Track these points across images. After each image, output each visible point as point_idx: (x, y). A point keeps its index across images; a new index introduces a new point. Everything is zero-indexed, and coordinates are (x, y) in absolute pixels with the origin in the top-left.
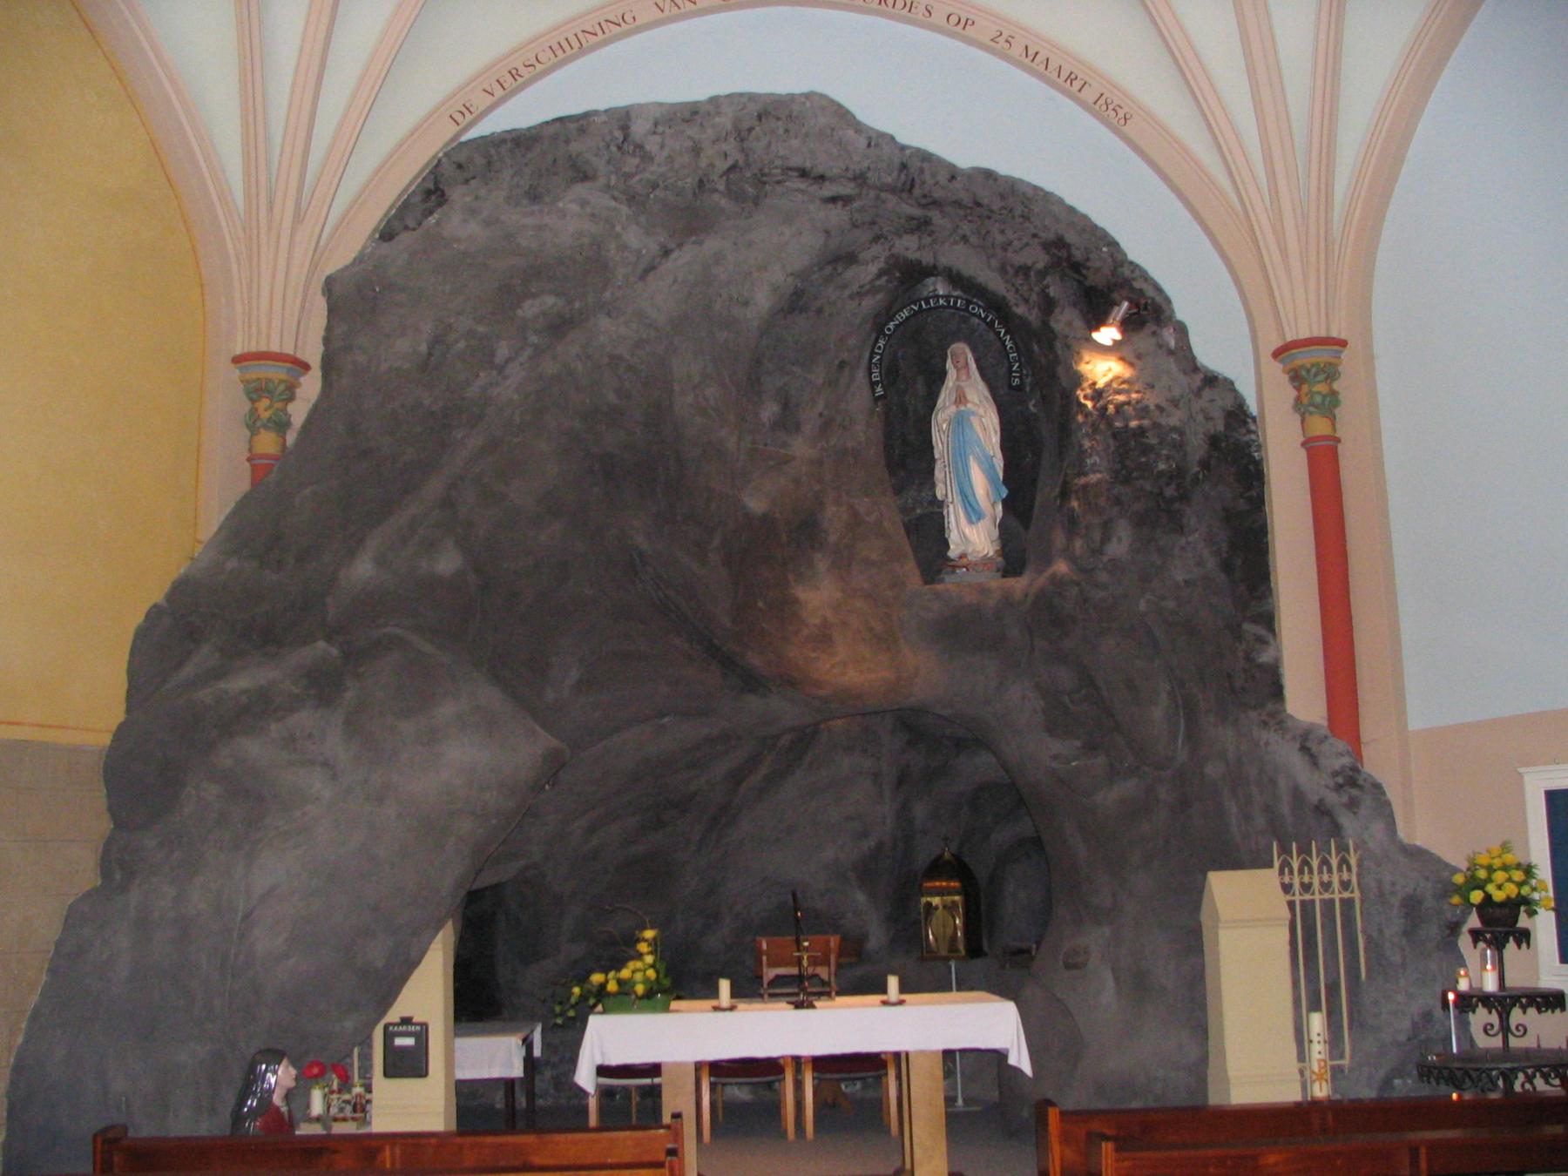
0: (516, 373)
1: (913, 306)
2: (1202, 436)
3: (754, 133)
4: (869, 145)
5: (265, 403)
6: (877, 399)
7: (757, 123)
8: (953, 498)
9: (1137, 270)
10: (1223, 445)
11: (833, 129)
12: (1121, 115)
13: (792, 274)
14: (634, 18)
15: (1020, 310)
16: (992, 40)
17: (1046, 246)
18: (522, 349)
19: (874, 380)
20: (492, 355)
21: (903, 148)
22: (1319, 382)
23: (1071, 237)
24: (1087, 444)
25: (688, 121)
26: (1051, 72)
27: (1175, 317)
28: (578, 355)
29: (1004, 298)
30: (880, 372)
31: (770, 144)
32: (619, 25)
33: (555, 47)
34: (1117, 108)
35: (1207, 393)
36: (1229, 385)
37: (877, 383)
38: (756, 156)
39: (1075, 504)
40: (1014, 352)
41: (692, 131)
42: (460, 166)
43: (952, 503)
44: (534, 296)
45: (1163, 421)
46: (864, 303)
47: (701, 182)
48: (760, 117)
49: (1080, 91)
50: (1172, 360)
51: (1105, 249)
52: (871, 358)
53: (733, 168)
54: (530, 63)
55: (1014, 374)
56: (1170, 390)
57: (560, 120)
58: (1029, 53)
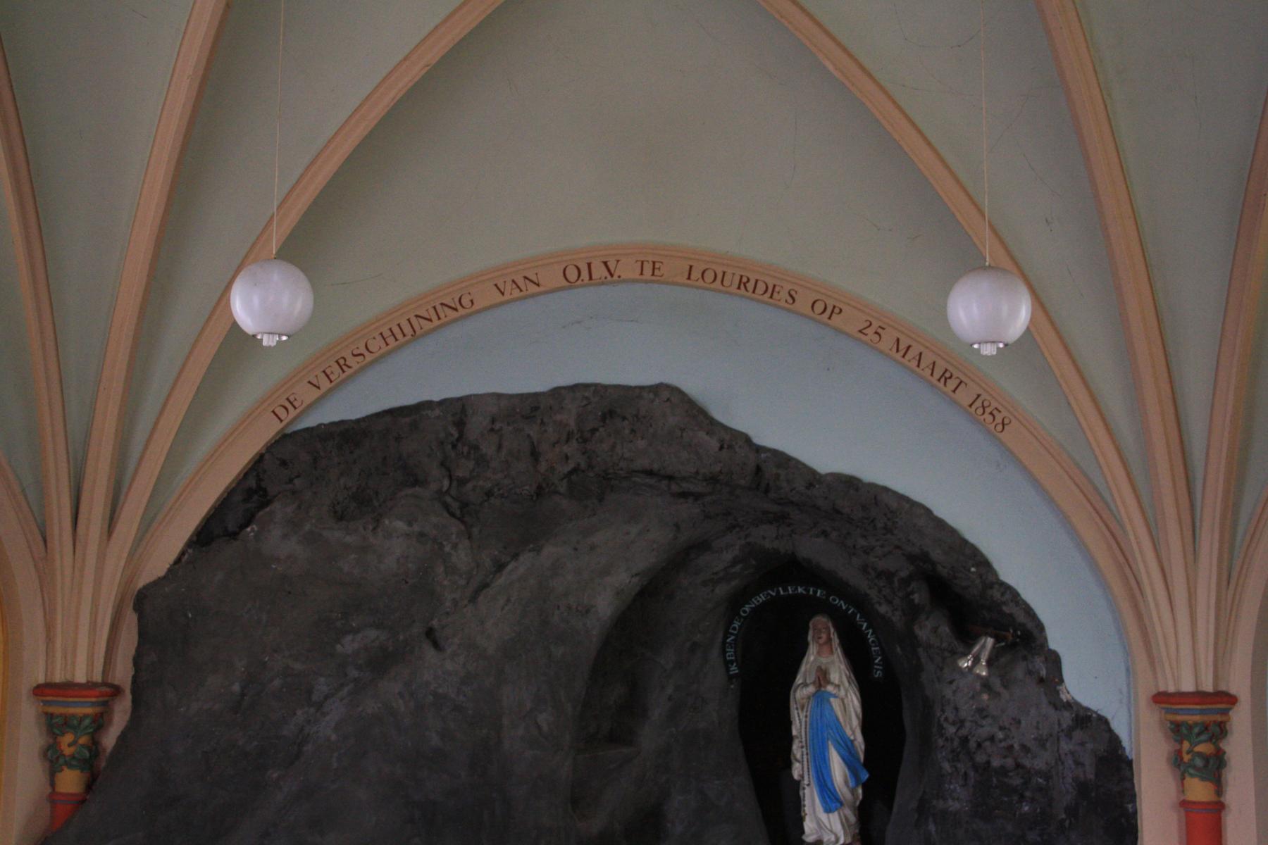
0: (336, 711)
1: (770, 592)
2: (1071, 781)
3: (597, 434)
4: (721, 448)
5: (68, 738)
6: (731, 678)
7: (602, 424)
8: (809, 781)
9: (1008, 592)
10: (1093, 794)
11: (683, 430)
12: (999, 419)
13: (636, 575)
14: (472, 302)
15: (883, 609)
16: (860, 331)
17: (911, 558)
18: (342, 685)
19: (728, 658)
20: (310, 692)
21: (759, 449)
22: (1201, 742)
23: (936, 554)
24: (947, 766)
25: (527, 418)
26: (923, 370)
27: (1048, 646)
28: (400, 693)
29: (866, 595)
30: (735, 652)
31: (613, 447)
32: (456, 309)
33: (387, 333)
34: (995, 412)
35: (1078, 735)
36: (1104, 721)
37: (732, 662)
38: (599, 459)
39: (932, 827)
40: (876, 646)
41: (533, 430)
42: (284, 463)
43: (808, 785)
44: (356, 631)
45: (1027, 762)
46: (717, 591)
47: (540, 487)
48: (603, 419)
49: (954, 391)
50: (1042, 689)
51: (973, 569)
52: (725, 637)
53: (575, 470)
54: (359, 352)
55: (876, 667)
56: (1037, 728)
57: (390, 412)
58: (900, 348)
